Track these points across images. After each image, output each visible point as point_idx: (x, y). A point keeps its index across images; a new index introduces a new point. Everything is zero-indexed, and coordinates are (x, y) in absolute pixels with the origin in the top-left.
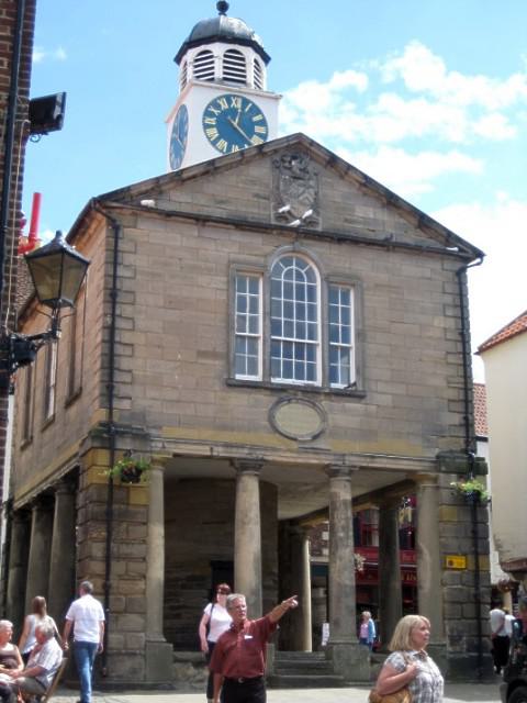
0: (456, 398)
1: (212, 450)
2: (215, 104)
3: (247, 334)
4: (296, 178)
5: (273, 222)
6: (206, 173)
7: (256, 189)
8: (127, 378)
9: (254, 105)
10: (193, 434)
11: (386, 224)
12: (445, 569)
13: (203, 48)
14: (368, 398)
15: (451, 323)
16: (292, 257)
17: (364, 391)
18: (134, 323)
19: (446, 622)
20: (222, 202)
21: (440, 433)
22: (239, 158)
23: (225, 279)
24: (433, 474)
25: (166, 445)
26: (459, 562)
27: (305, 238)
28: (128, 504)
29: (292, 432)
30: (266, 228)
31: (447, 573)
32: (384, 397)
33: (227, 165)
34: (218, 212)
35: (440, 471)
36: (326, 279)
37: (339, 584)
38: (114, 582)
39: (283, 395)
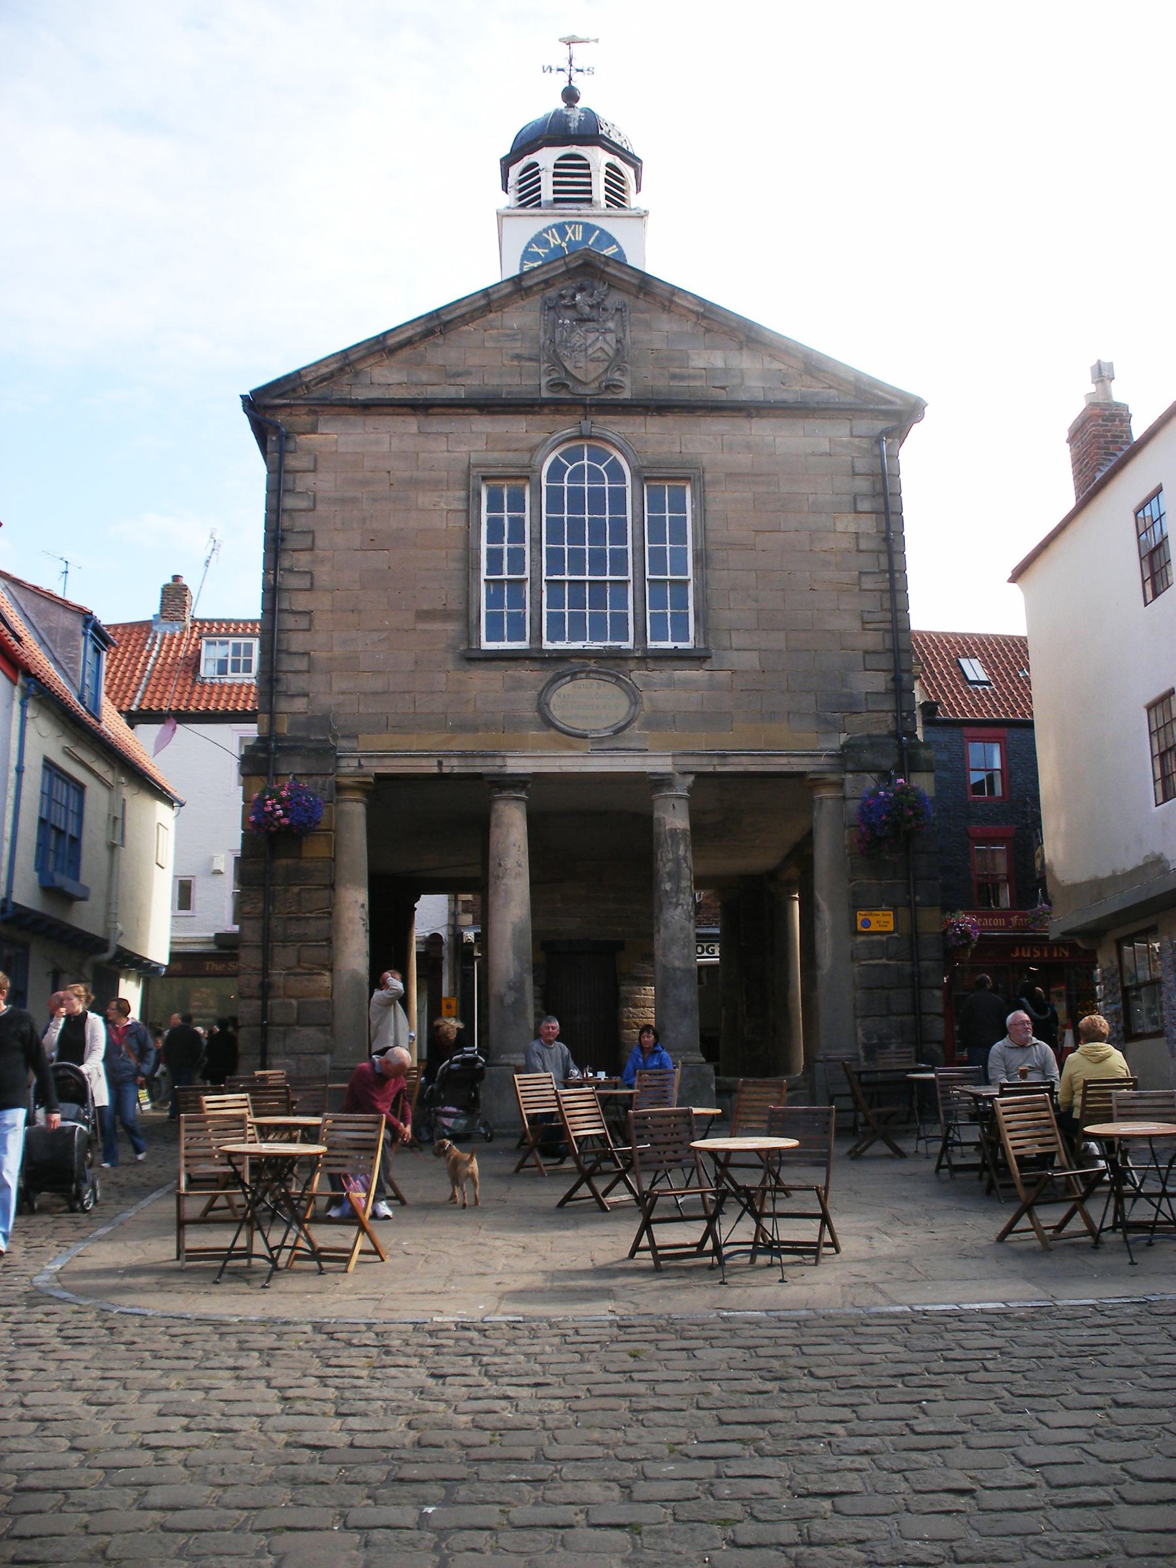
0: (880, 648)
1: (440, 764)
2: (539, 240)
3: (505, 576)
4: (582, 320)
5: (545, 394)
6: (428, 334)
7: (518, 347)
8: (301, 664)
9: (602, 231)
10: (412, 742)
11: (1167, 1118)
12: (856, 933)
13: (527, 160)
14: (714, 659)
15: (868, 524)
16: (583, 446)
17: (707, 649)
18: (312, 578)
19: (858, 1020)
20: (459, 375)
21: (850, 706)
22: (483, 302)
23: (463, 494)
24: (833, 777)
25: (363, 762)
26: (882, 921)
27: (599, 413)
28: (300, 858)
29: (579, 725)
30: (532, 406)
31: (861, 939)
32: (746, 655)
33: (462, 316)
34: (451, 392)
35: (847, 771)
36: (641, 477)
37: (664, 967)
38: (277, 976)
39: (563, 667)
